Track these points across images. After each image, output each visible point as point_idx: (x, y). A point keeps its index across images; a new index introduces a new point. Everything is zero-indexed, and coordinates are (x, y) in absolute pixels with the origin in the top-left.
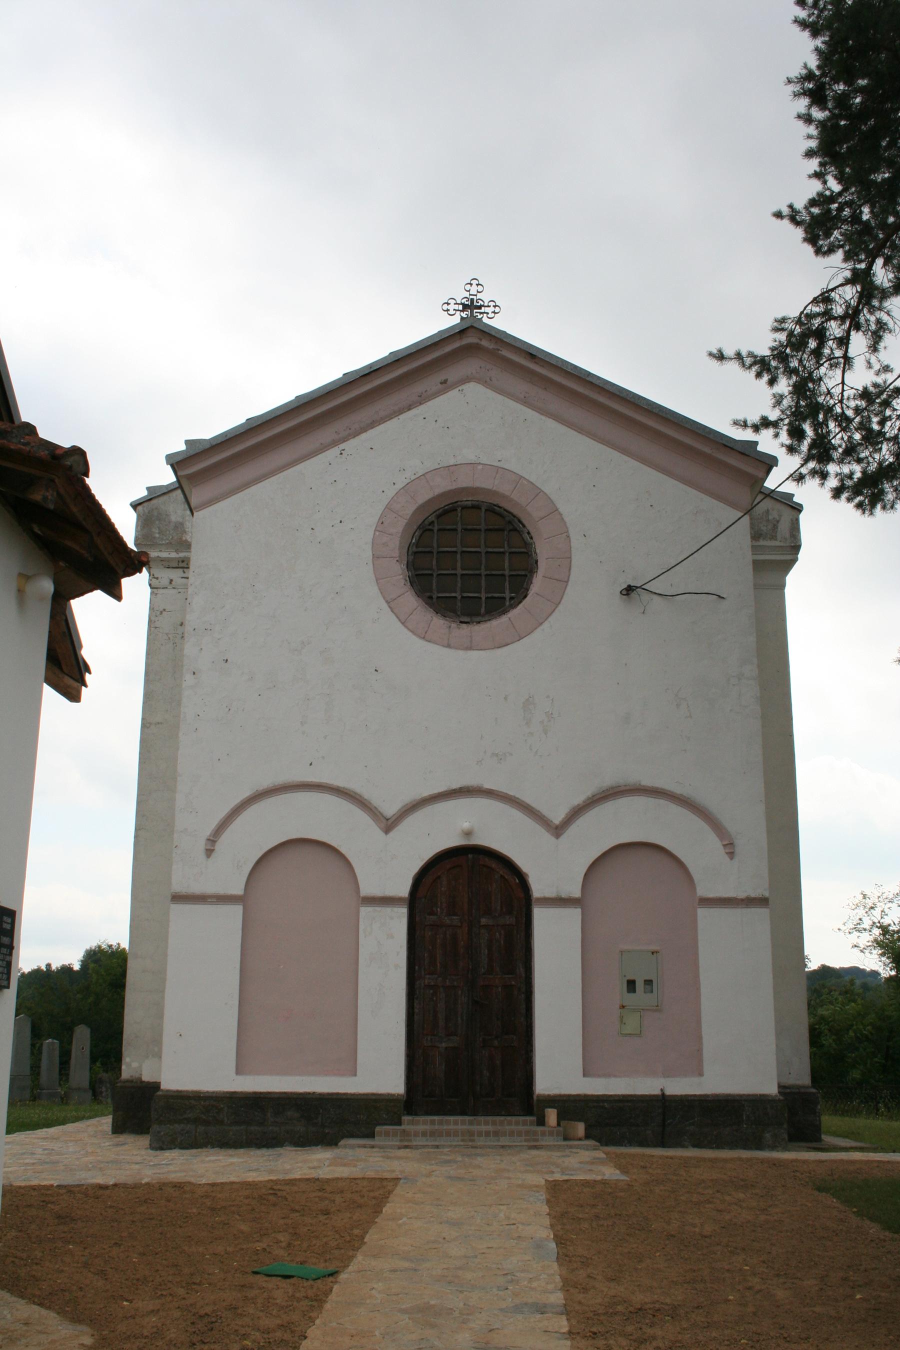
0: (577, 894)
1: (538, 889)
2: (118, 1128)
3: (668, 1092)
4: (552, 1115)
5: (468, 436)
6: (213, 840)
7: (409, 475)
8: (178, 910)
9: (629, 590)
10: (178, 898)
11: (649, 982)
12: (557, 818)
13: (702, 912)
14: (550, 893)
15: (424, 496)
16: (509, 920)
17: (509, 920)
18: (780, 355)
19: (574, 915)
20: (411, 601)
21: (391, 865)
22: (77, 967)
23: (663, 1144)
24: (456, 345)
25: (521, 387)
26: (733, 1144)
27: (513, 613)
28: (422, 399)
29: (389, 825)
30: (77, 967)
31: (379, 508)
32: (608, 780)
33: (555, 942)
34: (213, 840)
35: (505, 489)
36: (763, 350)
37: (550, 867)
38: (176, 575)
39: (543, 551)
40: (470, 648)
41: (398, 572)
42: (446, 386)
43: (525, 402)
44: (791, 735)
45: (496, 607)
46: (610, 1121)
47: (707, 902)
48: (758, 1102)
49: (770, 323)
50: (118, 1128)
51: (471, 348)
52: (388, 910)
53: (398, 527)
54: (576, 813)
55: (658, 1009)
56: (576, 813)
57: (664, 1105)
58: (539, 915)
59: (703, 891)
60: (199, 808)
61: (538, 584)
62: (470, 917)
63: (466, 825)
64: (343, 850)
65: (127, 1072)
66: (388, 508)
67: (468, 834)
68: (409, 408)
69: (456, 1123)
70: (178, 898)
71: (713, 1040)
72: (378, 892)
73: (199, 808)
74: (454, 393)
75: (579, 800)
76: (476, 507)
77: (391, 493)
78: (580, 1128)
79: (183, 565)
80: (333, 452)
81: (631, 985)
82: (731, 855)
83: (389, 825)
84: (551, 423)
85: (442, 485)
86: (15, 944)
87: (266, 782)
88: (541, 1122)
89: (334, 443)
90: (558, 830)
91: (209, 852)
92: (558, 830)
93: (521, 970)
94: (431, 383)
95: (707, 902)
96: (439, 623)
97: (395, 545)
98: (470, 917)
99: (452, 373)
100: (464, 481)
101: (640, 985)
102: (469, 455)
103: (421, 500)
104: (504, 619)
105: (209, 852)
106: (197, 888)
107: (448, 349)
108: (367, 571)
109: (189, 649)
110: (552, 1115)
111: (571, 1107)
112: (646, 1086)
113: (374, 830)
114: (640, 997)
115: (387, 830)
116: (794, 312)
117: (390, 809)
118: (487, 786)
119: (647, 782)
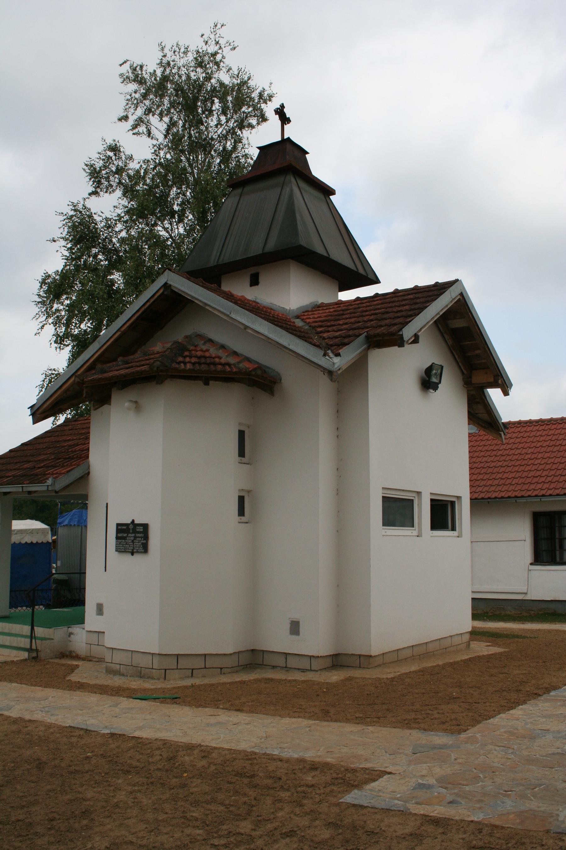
101: (423, 513)
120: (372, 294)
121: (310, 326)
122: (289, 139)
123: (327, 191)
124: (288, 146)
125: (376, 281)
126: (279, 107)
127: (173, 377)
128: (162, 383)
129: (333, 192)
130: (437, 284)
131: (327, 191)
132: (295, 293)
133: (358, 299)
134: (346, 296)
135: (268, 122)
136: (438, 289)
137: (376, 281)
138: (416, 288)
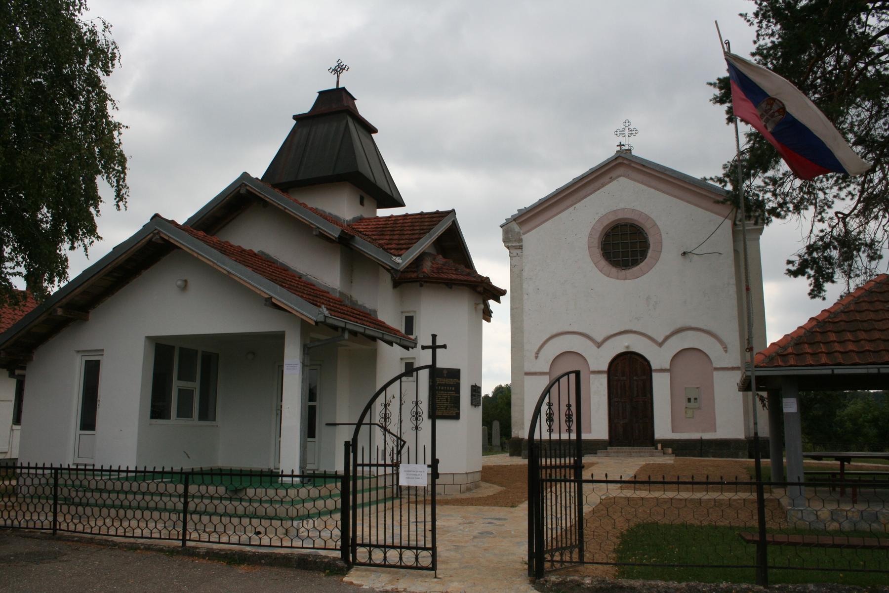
0: (668, 367)
1: (653, 367)
2: (511, 455)
3: (704, 438)
4: (659, 446)
5: (624, 198)
6: (537, 353)
7: (600, 215)
8: (527, 378)
9: (684, 253)
10: (527, 374)
11: (696, 399)
12: (660, 340)
13: (715, 373)
14: (658, 367)
15: (606, 223)
16: (644, 377)
17: (644, 377)
18: (726, 175)
19: (667, 375)
20: (603, 263)
21: (600, 359)
22: (490, 396)
23: (701, 456)
24: (614, 164)
25: (640, 177)
26: (728, 456)
27: (642, 264)
28: (603, 185)
29: (599, 345)
30: (490, 396)
31: (590, 229)
32: (679, 325)
33: (661, 386)
34: (537, 353)
35: (636, 218)
36: (721, 176)
37: (658, 358)
38: (519, 251)
39: (651, 240)
40: (626, 279)
41: (598, 252)
42: (612, 179)
43: (642, 183)
44: (763, 300)
45: (635, 263)
46: (681, 448)
47: (716, 369)
48: (737, 441)
49: (721, 166)
50: (511, 455)
51: (623, 163)
52: (600, 375)
53: (597, 235)
54: (667, 338)
55: (699, 408)
56: (667, 338)
57: (701, 442)
58: (654, 375)
59: (715, 365)
60: (532, 344)
61: (650, 253)
62: (630, 377)
63: (626, 344)
64: (583, 354)
65: (513, 435)
66: (593, 228)
67: (627, 347)
68: (598, 189)
69: (626, 449)
70: (527, 374)
71: (719, 420)
72: (596, 369)
73: (532, 344)
74: (615, 182)
75: (668, 333)
76: (626, 225)
77: (594, 222)
78: (670, 450)
79: (521, 247)
80: (571, 209)
81: (689, 400)
82: (726, 351)
83: (599, 345)
84: (652, 190)
85: (612, 218)
86: (92, 314)
87: (555, 332)
88: (657, 448)
89: (572, 205)
90: (660, 345)
91: (536, 358)
92: (660, 345)
93: (649, 395)
94: (606, 179)
95: (716, 369)
96: (614, 270)
97: (596, 242)
98: (630, 377)
99: (613, 174)
100: (621, 216)
101: (692, 400)
102: (622, 206)
103: (605, 225)
104: (638, 267)
105: (536, 358)
106: (533, 370)
107: (611, 165)
108: (587, 253)
109: (525, 286)
110: (659, 446)
111: (666, 443)
112: (695, 436)
113: (594, 348)
114: (693, 404)
115: (599, 347)
116: (731, 160)
117: (599, 339)
118: (634, 329)
119: (693, 326)
120: (389, 215)
121: (857, 216)
122: (344, 89)
123: (371, 130)
124: (343, 93)
125: (401, 204)
126: (727, 116)
127: (405, 282)
128: (86, 319)
129: (375, 131)
130: (437, 212)
131: (371, 130)
132: (343, 207)
133: (392, 216)
134: (382, 213)
135: (726, 121)
136: (438, 216)
137: (401, 204)
138: (422, 214)
